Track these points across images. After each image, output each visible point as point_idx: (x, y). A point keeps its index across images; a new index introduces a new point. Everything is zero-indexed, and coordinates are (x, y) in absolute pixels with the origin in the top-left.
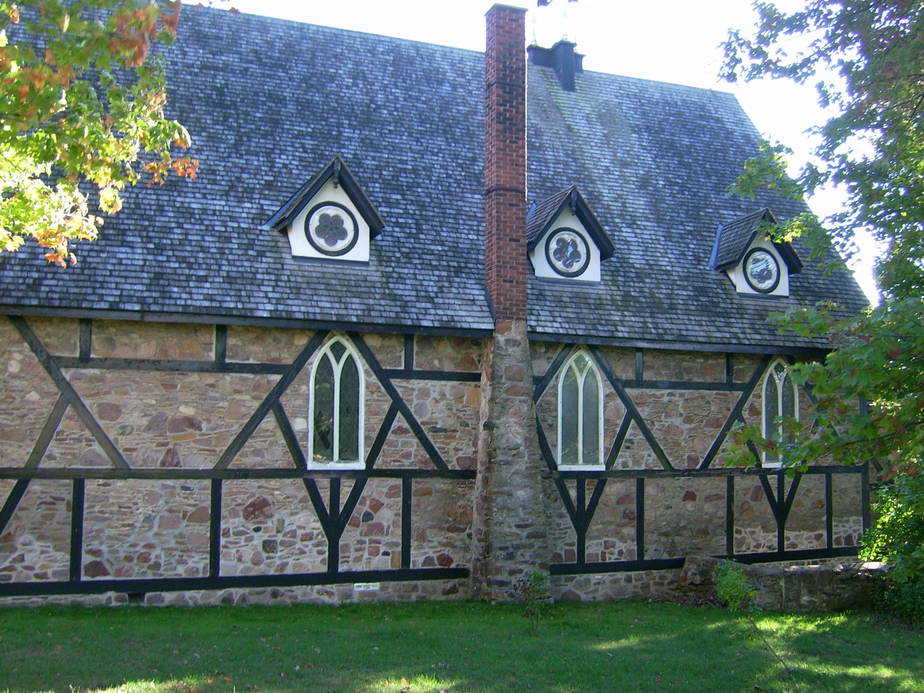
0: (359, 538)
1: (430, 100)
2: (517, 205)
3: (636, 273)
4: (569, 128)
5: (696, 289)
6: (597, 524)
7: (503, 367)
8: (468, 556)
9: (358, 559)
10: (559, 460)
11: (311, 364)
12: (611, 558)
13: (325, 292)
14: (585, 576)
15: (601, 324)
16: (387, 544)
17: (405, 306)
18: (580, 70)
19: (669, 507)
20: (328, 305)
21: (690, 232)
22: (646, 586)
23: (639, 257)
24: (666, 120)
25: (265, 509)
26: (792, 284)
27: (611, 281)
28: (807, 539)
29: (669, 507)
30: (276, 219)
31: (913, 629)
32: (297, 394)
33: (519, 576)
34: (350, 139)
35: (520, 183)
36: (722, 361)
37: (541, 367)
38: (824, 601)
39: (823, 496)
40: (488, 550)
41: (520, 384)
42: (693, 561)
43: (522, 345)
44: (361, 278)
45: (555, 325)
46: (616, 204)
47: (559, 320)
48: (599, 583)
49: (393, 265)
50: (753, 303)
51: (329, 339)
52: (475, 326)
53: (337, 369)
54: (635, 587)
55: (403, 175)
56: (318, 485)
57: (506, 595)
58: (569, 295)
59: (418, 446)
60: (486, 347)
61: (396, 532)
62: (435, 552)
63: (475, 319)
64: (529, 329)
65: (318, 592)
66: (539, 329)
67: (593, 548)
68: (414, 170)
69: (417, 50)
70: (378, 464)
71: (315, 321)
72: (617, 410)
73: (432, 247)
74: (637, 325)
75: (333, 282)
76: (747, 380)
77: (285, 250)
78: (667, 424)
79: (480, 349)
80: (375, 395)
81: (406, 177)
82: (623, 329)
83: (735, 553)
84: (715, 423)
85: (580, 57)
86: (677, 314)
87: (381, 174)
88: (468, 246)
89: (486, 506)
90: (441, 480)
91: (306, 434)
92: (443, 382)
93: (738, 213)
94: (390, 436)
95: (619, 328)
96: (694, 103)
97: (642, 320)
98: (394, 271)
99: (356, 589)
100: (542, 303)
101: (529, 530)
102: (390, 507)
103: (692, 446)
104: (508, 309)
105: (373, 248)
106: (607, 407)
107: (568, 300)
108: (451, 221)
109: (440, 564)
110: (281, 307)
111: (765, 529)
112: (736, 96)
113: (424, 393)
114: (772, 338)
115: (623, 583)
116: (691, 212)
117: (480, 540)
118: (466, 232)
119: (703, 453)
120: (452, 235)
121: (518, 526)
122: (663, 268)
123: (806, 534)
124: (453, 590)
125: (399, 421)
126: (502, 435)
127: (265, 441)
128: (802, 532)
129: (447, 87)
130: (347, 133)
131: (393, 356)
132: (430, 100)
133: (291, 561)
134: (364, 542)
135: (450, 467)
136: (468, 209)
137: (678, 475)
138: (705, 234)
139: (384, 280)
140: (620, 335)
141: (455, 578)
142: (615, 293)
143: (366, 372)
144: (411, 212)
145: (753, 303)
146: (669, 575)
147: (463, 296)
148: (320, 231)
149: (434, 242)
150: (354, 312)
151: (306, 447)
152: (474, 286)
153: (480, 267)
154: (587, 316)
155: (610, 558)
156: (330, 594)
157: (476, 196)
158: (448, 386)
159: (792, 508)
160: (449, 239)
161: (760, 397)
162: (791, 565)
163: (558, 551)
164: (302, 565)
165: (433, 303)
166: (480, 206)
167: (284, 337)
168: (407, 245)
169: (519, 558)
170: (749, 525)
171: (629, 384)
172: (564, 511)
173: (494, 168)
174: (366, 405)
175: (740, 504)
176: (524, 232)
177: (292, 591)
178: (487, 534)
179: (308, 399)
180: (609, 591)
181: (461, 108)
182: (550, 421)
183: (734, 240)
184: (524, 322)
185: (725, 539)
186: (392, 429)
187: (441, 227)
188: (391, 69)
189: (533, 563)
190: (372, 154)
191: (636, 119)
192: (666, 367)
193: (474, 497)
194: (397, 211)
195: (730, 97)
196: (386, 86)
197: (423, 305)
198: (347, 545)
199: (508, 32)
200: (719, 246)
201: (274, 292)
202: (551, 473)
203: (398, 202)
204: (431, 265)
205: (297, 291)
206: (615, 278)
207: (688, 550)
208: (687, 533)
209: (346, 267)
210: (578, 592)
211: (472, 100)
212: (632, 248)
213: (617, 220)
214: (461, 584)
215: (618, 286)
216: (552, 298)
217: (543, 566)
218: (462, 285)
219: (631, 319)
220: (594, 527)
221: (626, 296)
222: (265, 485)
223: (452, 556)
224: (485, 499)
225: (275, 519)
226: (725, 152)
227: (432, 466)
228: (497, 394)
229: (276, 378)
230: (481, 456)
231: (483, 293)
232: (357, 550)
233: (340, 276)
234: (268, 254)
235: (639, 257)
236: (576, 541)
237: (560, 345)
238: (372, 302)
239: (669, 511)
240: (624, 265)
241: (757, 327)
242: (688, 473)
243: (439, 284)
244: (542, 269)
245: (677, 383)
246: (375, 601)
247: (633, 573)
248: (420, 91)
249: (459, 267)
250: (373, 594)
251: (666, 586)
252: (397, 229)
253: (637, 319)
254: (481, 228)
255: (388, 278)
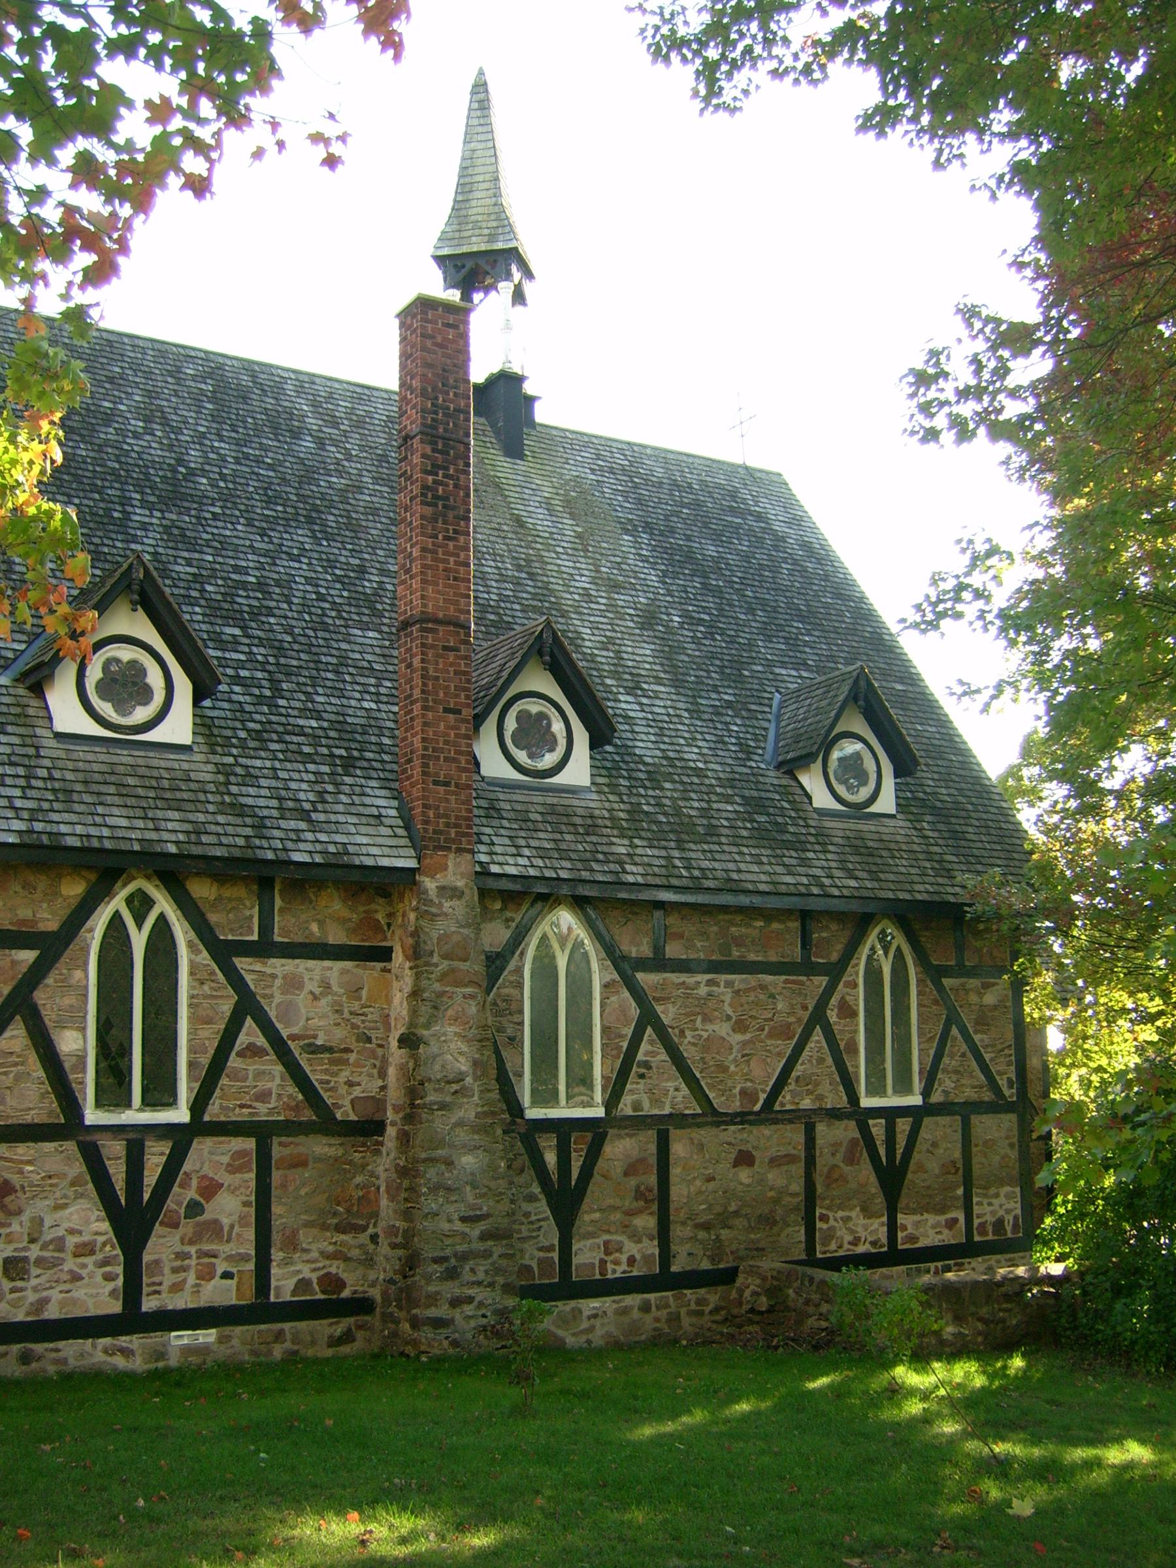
0: (178, 1248)
1: (281, 463)
2: (457, 650)
3: (648, 772)
4: (519, 522)
5: (747, 801)
6: (593, 1211)
7: (435, 935)
8: (372, 1275)
9: (177, 1288)
10: (526, 1100)
11: (92, 930)
12: (615, 1271)
13: (117, 800)
14: (573, 1303)
15: (598, 861)
16: (229, 1258)
17: (260, 826)
18: (532, 424)
19: (710, 1179)
20: (124, 822)
21: (729, 705)
22: (674, 1319)
23: (650, 745)
24: (677, 514)
25: (7, 1200)
26: (901, 795)
27: (608, 785)
28: (933, 1227)
29: (710, 1179)
30: (20, 666)
31: (1134, 1375)
32: (65, 985)
33: (469, 1309)
34: (144, 527)
35: (461, 611)
36: (795, 925)
37: (496, 934)
38: (980, 1333)
39: (957, 1154)
40: (411, 1263)
41: (464, 966)
42: (753, 1271)
43: (467, 897)
44: (179, 774)
45: (521, 861)
46: (605, 653)
47: (526, 852)
48: (595, 1316)
49: (235, 751)
50: (840, 825)
51: (125, 885)
52: (385, 862)
53: (139, 940)
54: (657, 1320)
55: (241, 592)
56: (105, 1152)
57: (446, 1343)
58: (540, 809)
59: (282, 1079)
60: (402, 900)
61: (245, 1236)
62: (314, 1270)
63: (384, 850)
64: (478, 869)
65: (106, 1351)
66: (495, 869)
67: (586, 1254)
68: (261, 585)
69: (254, 376)
70: (214, 1112)
71: (102, 851)
72: (624, 1011)
73: (301, 722)
74: (657, 862)
75: (131, 781)
76: (835, 957)
77: (41, 722)
78: (705, 1035)
79: (390, 903)
80: (206, 988)
81: (248, 597)
82: (634, 869)
83: (819, 1255)
84: (784, 1032)
85: (530, 400)
86: (720, 844)
87: (203, 591)
88: (363, 721)
89: (406, 1183)
90: (325, 1140)
91: (82, 1059)
92: (327, 963)
93: (804, 674)
94: (234, 1062)
95: (628, 867)
96: (719, 486)
97: (663, 853)
98: (237, 764)
99: (174, 1342)
100: (496, 823)
101: (482, 1226)
102: (233, 1191)
103: (744, 1073)
104: (441, 832)
105: (198, 721)
106: (606, 1007)
107: (539, 818)
108: (330, 675)
109: (323, 1292)
110: (39, 826)
111: (867, 1212)
112: (787, 477)
113: (293, 984)
114: (876, 885)
115: (636, 1314)
116: (728, 671)
117: (394, 1246)
118: (358, 695)
119: (765, 1083)
120: (333, 700)
121: (463, 1219)
122: (692, 764)
123: (932, 1218)
124: (348, 1337)
125: (250, 1034)
126: (434, 1057)
127: (5, 1073)
128: (926, 1215)
129: (308, 443)
130: (139, 515)
131: (239, 918)
132: (281, 463)
133: (55, 1295)
134: (187, 1256)
135: (339, 1116)
136: (358, 656)
137: (726, 1123)
138: (753, 707)
139: (221, 778)
140: (631, 879)
141: (351, 1315)
142: (616, 806)
143: (190, 945)
144: (259, 658)
145: (840, 825)
146: (713, 1297)
147: (362, 810)
148: (104, 688)
149: (304, 712)
150: (171, 834)
151: (82, 1082)
152: (378, 792)
153: (386, 757)
154: (573, 847)
155: (614, 1271)
156: (126, 1352)
157: (371, 634)
158: (335, 969)
159: (910, 1176)
160: (328, 708)
161: (856, 986)
162: (948, 1269)
163: (526, 1262)
164: (74, 1302)
165: (310, 821)
166: (378, 650)
167: (41, 882)
168: (257, 717)
169: (467, 1276)
170: (841, 1207)
171: (642, 964)
172: (536, 1189)
173: (416, 583)
174: (190, 1006)
175: (825, 1170)
176: (467, 697)
177: (57, 1350)
178: (409, 1234)
179: (86, 996)
180: (612, 1329)
181: (334, 480)
182: (510, 1031)
183: (806, 719)
184: (469, 856)
185: (803, 1231)
186: (237, 1047)
187: (313, 686)
188: (210, 406)
189: (491, 1285)
190: (186, 554)
191: (627, 511)
192: (704, 934)
193: (381, 1168)
194: (235, 656)
195: (775, 478)
196: (203, 436)
197: (293, 824)
198: (157, 1262)
199: (441, 346)
200: (777, 728)
201: (24, 797)
202: (514, 1123)
203: (235, 640)
204: (301, 753)
205: (66, 795)
206: (614, 781)
207: (742, 1253)
208: (739, 1222)
209: (151, 754)
210: (560, 1333)
211: (352, 467)
212: (637, 729)
213: (609, 681)
214: (360, 1327)
215: (620, 795)
216: (512, 815)
217: (507, 1289)
218: (357, 790)
219: (644, 851)
220: (588, 1216)
221: (635, 812)
222: (7, 1155)
223: (344, 1276)
224: (403, 1172)
225: (25, 1217)
226: (775, 570)
227: (308, 1115)
228: (424, 983)
229: (28, 956)
230: (395, 1094)
231: (395, 803)
232: (175, 1270)
233: (142, 771)
234: (10, 729)
235: (650, 745)
236: (556, 1242)
237: (534, 895)
238: (201, 817)
239: (712, 1185)
240: (627, 758)
241: (850, 866)
242: (741, 1118)
243: (318, 788)
244: (494, 765)
245: (721, 962)
246: (209, 1364)
247: (652, 1297)
248: (262, 447)
249: (350, 757)
250: (204, 1350)
251: (707, 1318)
252: (237, 689)
253: (656, 852)
254: (383, 690)
255: (227, 775)
